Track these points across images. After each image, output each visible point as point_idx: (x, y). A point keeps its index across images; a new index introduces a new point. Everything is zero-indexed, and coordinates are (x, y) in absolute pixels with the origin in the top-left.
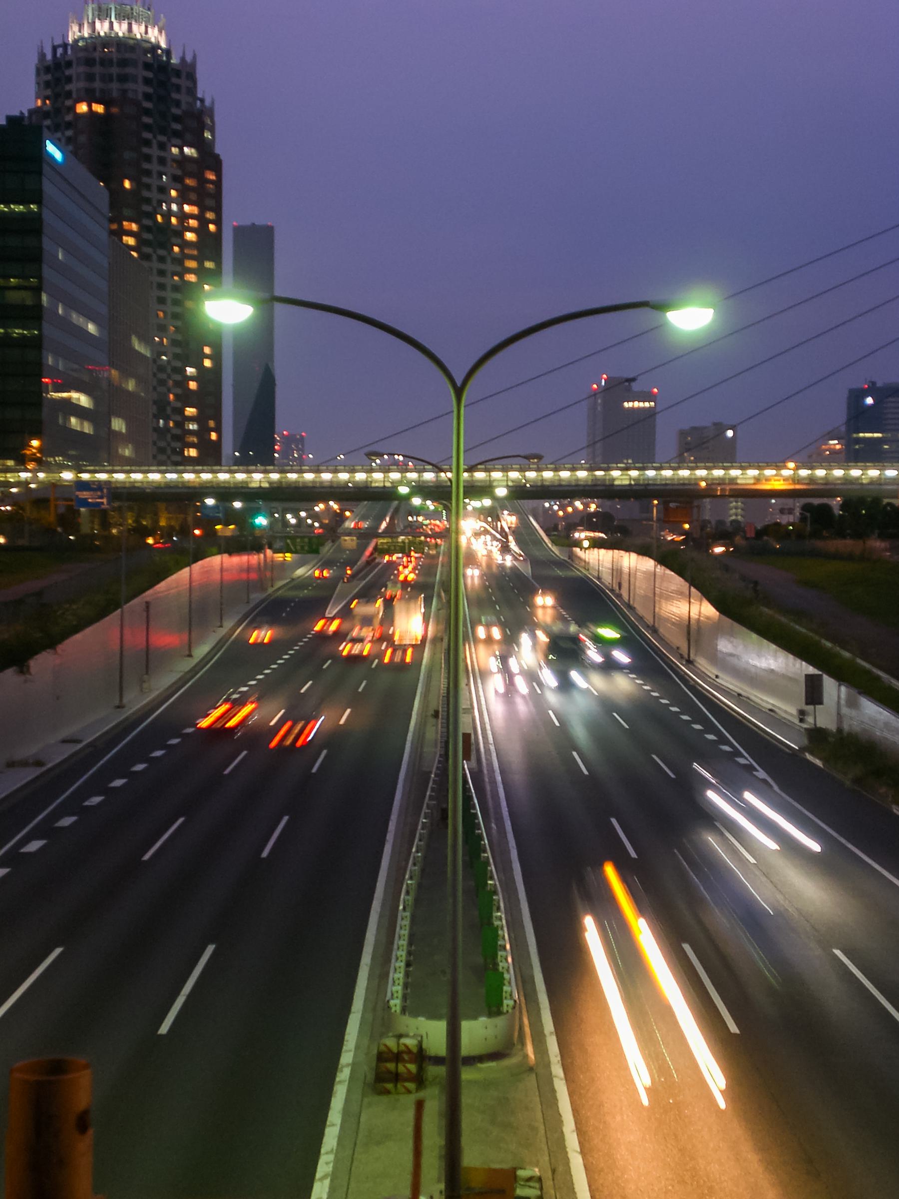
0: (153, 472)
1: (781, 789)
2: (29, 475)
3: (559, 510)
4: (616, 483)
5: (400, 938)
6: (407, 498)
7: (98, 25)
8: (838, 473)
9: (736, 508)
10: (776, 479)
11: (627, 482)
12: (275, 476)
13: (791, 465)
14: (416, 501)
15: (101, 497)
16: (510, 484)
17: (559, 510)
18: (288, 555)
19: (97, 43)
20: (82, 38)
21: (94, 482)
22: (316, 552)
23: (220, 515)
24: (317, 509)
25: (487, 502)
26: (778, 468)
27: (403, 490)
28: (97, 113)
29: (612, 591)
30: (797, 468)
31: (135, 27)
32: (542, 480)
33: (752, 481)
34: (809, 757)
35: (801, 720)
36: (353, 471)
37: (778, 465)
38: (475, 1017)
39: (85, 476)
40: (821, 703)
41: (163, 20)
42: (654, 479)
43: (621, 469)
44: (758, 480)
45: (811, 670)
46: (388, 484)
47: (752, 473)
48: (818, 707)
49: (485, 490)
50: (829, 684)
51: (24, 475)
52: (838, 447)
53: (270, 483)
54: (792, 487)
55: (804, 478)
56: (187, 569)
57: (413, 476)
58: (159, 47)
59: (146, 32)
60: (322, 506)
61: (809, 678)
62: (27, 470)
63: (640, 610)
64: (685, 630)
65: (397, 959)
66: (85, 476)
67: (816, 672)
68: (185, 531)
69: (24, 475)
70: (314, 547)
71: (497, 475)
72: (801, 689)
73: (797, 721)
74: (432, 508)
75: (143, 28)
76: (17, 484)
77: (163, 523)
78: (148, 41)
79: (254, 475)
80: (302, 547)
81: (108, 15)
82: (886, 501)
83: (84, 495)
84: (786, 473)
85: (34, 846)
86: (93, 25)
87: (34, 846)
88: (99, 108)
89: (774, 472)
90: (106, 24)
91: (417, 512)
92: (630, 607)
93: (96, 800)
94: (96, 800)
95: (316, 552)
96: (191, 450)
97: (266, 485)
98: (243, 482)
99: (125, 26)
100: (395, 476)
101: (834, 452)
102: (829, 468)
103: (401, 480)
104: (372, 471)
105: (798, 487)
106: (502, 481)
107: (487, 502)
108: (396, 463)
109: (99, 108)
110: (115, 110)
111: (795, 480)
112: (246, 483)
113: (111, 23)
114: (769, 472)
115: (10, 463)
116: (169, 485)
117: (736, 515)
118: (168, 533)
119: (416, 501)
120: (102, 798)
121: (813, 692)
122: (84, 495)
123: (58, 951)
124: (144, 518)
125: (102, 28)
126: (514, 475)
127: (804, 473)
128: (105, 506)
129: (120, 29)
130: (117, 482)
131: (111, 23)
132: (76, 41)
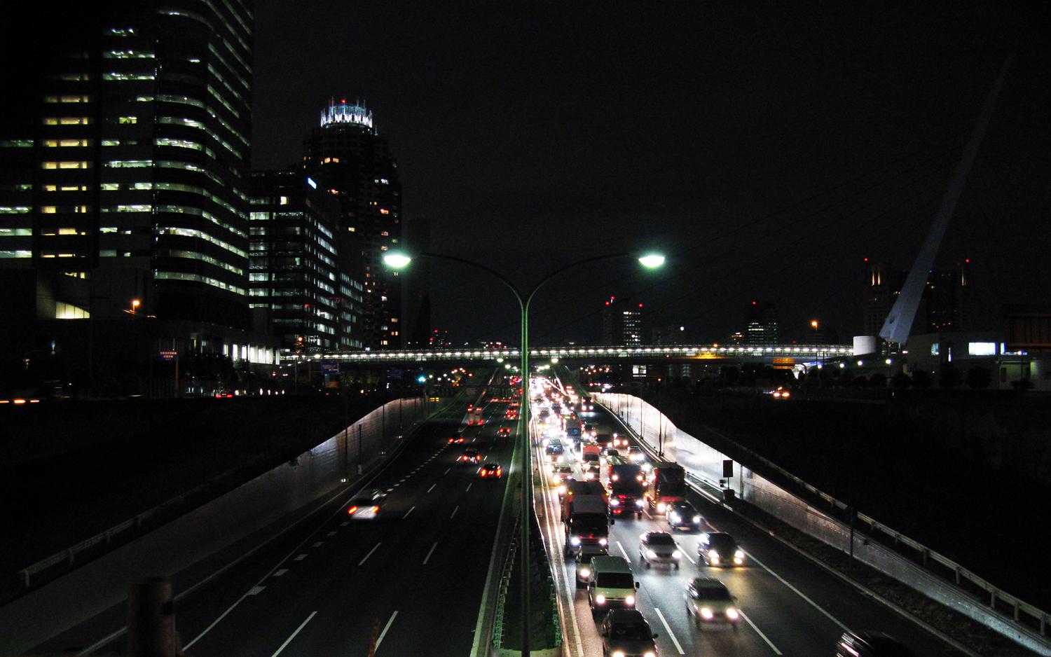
0: (345, 354)
1: (710, 523)
2: (297, 356)
3: (450, 381)
4: (620, 356)
5: (499, 602)
6: (502, 365)
7: (336, 116)
8: (741, 350)
9: (686, 370)
10: (708, 353)
11: (626, 356)
12: (429, 355)
13: (716, 345)
14: (508, 367)
15: (336, 368)
16: (561, 357)
17: (450, 381)
18: (437, 398)
19: (336, 126)
20: (327, 124)
21: (332, 360)
22: (453, 396)
23: (400, 377)
24: (453, 372)
25: (547, 367)
26: (709, 348)
27: (500, 360)
28: (335, 162)
29: (618, 416)
30: (718, 348)
31: (356, 117)
32: (579, 355)
33: (694, 355)
34: (725, 505)
35: (722, 486)
36: (472, 351)
37: (708, 344)
38: (539, 649)
39: (327, 357)
40: (732, 476)
41: (371, 114)
42: (640, 354)
43: (623, 348)
44: (697, 354)
45: (727, 458)
46: (492, 358)
47: (695, 350)
48: (730, 478)
49: (546, 360)
50: (736, 466)
51: (294, 357)
52: (740, 336)
53: (427, 358)
54: (716, 358)
55: (722, 353)
56: (382, 407)
57: (506, 353)
58: (369, 128)
59: (362, 120)
60: (456, 371)
61: (725, 462)
62: (296, 354)
63: (634, 427)
64: (854, 548)
65: (497, 618)
66: (327, 357)
67: (727, 458)
68: (382, 386)
69: (294, 357)
70: (452, 394)
71: (553, 352)
72: (721, 469)
73: (719, 486)
74: (517, 370)
75: (360, 117)
76: (292, 362)
77: (369, 382)
78: (362, 124)
79: (418, 354)
80: (445, 394)
81: (341, 112)
82: (766, 365)
83: (326, 367)
84: (713, 350)
85: (301, 557)
86: (334, 117)
87: (301, 557)
88: (336, 160)
89: (706, 349)
90: (341, 116)
91: (509, 373)
92: (628, 425)
93: (319, 544)
94: (319, 544)
95: (453, 396)
96: (323, 331)
97: (424, 360)
98: (412, 358)
99: (350, 117)
100: (496, 353)
101: (738, 339)
102: (736, 347)
103: (498, 356)
104: (483, 351)
105: (718, 358)
106: (555, 356)
107: (547, 367)
108: (497, 346)
109: (336, 160)
110: (345, 161)
111: (716, 354)
112: (414, 359)
113: (343, 116)
114: (704, 349)
115: (288, 350)
116: (372, 361)
117: (687, 374)
118: (373, 386)
119: (508, 367)
120: (286, 570)
121: (728, 470)
122: (326, 367)
123: (315, 613)
124: (359, 379)
125: (338, 118)
126: (563, 352)
127: (722, 350)
128: (338, 373)
129: (348, 119)
130: (344, 359)
131: (343, 116)
132: (324, 126)
